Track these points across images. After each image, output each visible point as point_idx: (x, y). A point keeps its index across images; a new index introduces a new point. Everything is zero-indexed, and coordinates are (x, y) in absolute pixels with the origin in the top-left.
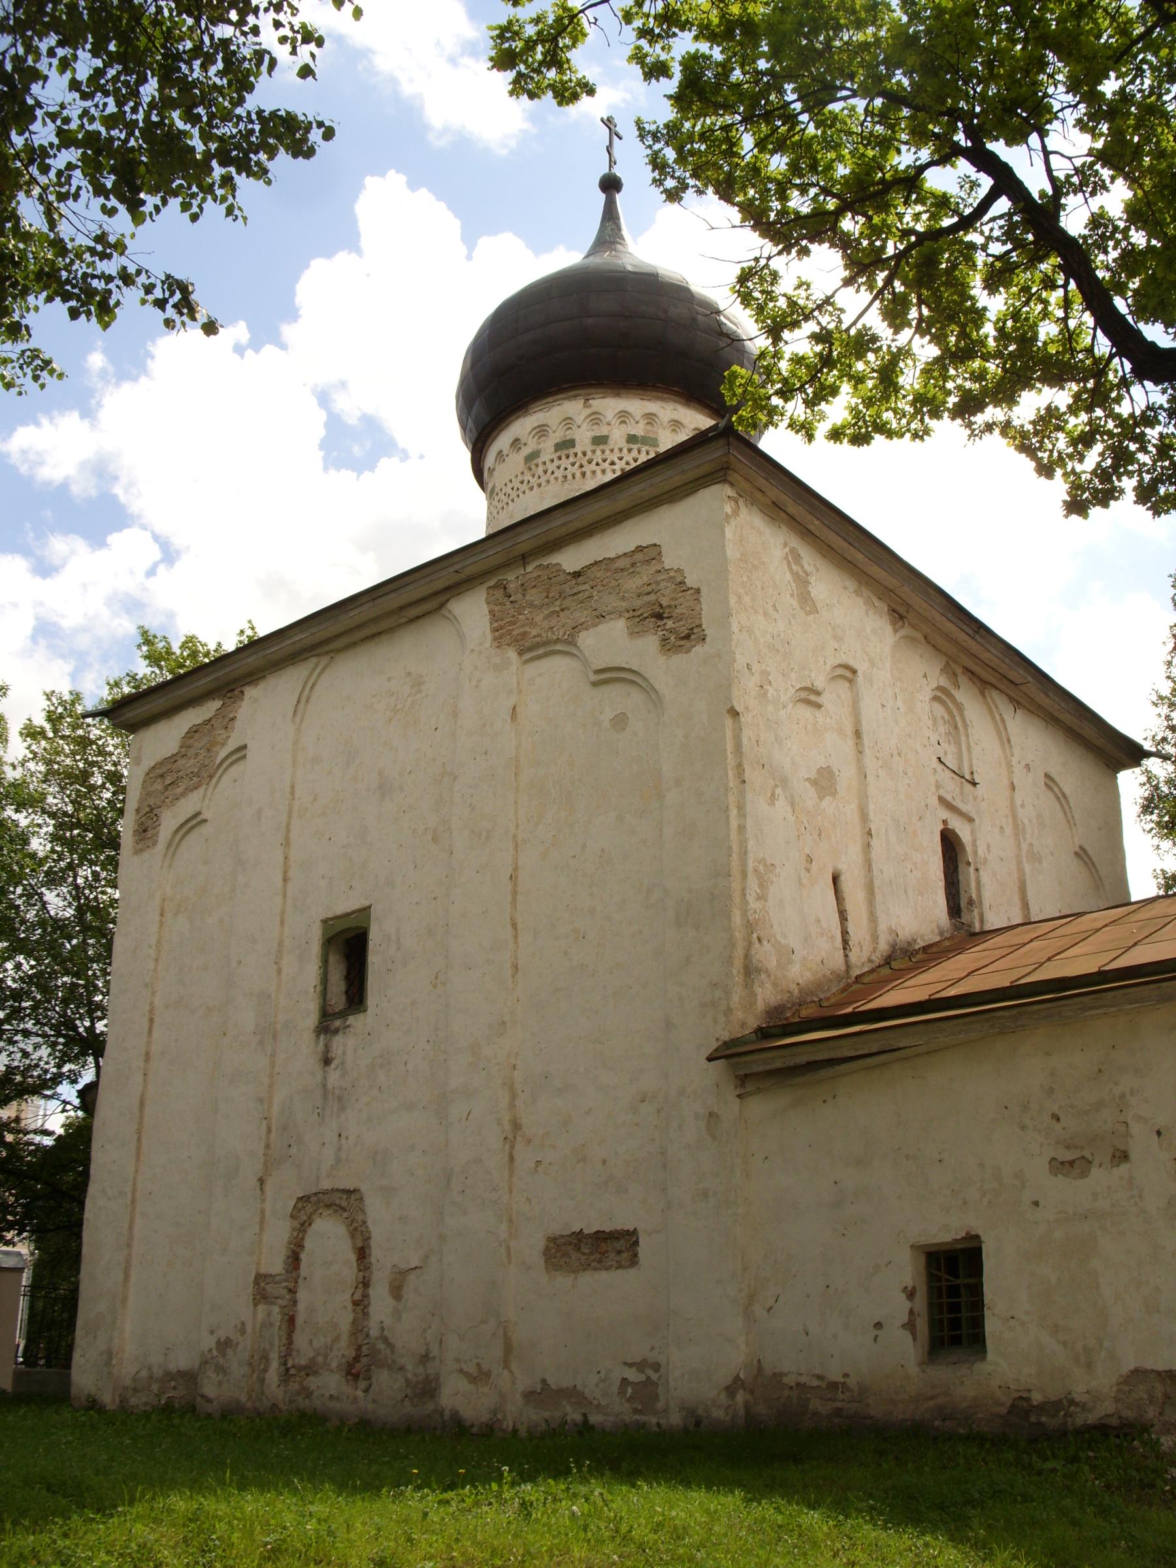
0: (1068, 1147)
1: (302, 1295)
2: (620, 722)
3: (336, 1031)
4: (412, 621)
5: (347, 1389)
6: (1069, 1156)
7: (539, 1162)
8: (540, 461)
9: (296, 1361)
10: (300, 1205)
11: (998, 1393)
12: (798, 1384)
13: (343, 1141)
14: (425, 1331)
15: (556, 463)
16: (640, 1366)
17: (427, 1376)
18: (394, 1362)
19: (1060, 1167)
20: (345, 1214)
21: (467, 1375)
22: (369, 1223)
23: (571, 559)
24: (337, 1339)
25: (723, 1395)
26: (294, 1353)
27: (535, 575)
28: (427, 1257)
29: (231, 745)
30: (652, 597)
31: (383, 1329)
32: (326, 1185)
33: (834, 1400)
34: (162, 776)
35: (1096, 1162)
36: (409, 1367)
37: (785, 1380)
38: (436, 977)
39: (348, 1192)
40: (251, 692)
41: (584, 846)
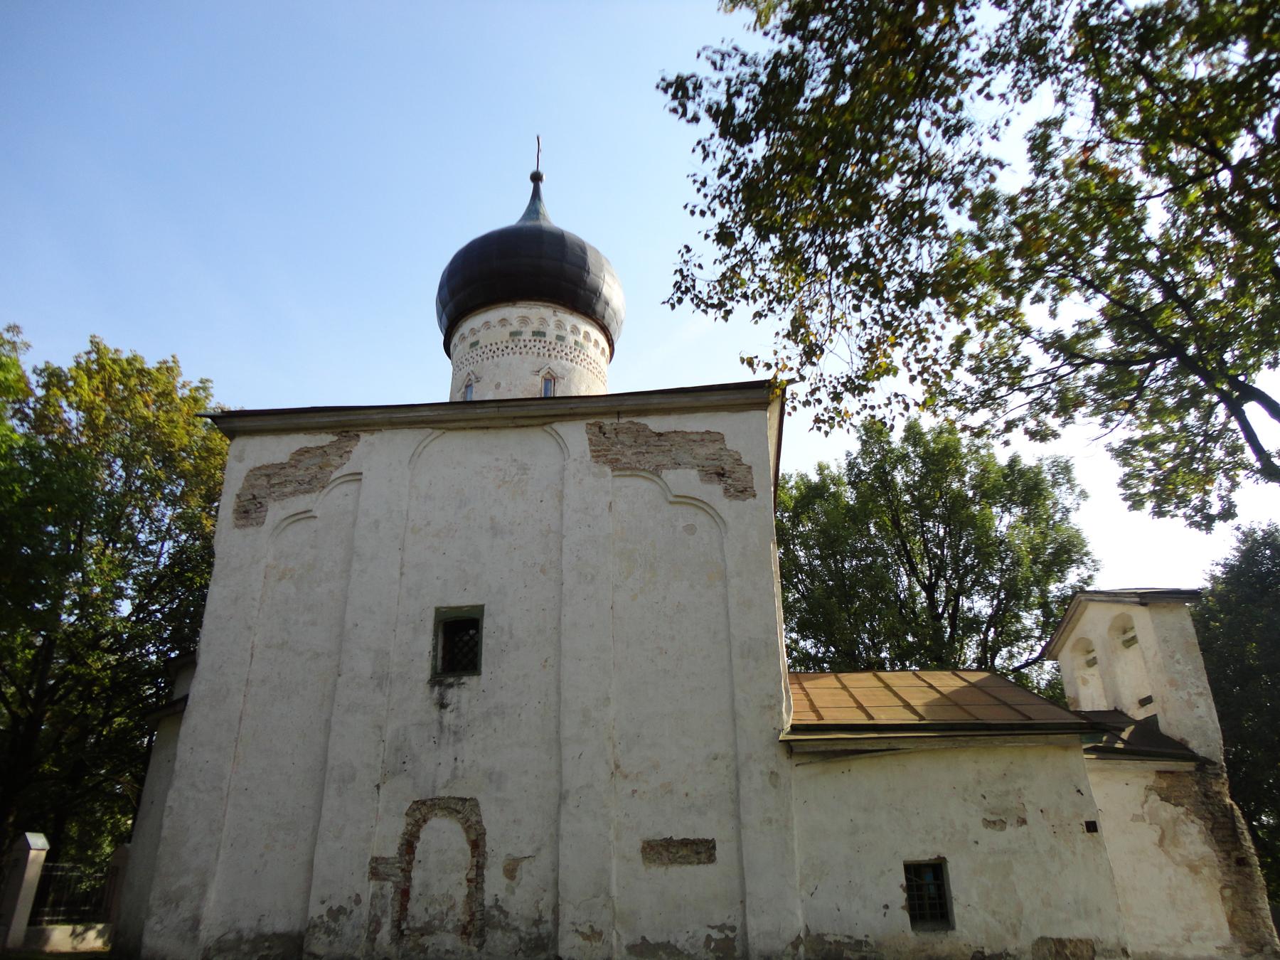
0: (992, 813)
1: (417, 875)
2: (691, 529)
3: (451, 686)
4: (517, 427)
5: (461, 944)
6: (993, 818)
7: (634, 791)
8: (522, 338)
9: (411, 925)
10: (415, 807)
11: (964, 948)
12: (835, 941)
13: (459, 763)
14: (538, 902)
15: (533, 343)
16: (721, 928)
17: (540, 935)
18: (508, 924)
19: (989, 824)
20: (460, 816)
21: (582, 934)
22: (485, 823)
23: (656, 423)
24: (453, 907)
25: (790, 948)
26: (409, 918)
27: (627, 426)
28: (539, 849)
29: (346, 469)
30: (717, 463)
31: (497, 900)
32: (443, 793)
33: (860, 951)
34: (268, 476)
35: (1009, 823)
36: (523, 928)
37: (826, 938)
38: (546, 661)
39: (464, 800)
40: (365, 437)
41: (665, 598)
